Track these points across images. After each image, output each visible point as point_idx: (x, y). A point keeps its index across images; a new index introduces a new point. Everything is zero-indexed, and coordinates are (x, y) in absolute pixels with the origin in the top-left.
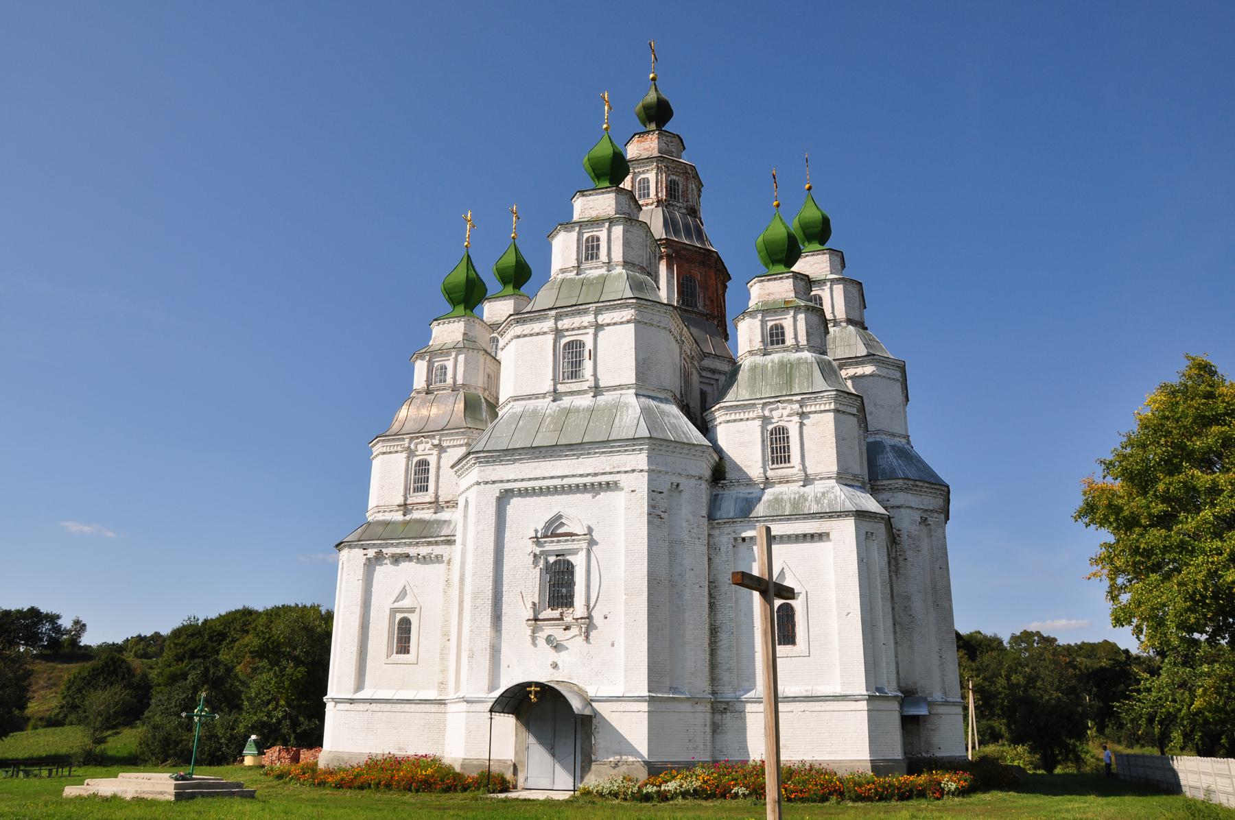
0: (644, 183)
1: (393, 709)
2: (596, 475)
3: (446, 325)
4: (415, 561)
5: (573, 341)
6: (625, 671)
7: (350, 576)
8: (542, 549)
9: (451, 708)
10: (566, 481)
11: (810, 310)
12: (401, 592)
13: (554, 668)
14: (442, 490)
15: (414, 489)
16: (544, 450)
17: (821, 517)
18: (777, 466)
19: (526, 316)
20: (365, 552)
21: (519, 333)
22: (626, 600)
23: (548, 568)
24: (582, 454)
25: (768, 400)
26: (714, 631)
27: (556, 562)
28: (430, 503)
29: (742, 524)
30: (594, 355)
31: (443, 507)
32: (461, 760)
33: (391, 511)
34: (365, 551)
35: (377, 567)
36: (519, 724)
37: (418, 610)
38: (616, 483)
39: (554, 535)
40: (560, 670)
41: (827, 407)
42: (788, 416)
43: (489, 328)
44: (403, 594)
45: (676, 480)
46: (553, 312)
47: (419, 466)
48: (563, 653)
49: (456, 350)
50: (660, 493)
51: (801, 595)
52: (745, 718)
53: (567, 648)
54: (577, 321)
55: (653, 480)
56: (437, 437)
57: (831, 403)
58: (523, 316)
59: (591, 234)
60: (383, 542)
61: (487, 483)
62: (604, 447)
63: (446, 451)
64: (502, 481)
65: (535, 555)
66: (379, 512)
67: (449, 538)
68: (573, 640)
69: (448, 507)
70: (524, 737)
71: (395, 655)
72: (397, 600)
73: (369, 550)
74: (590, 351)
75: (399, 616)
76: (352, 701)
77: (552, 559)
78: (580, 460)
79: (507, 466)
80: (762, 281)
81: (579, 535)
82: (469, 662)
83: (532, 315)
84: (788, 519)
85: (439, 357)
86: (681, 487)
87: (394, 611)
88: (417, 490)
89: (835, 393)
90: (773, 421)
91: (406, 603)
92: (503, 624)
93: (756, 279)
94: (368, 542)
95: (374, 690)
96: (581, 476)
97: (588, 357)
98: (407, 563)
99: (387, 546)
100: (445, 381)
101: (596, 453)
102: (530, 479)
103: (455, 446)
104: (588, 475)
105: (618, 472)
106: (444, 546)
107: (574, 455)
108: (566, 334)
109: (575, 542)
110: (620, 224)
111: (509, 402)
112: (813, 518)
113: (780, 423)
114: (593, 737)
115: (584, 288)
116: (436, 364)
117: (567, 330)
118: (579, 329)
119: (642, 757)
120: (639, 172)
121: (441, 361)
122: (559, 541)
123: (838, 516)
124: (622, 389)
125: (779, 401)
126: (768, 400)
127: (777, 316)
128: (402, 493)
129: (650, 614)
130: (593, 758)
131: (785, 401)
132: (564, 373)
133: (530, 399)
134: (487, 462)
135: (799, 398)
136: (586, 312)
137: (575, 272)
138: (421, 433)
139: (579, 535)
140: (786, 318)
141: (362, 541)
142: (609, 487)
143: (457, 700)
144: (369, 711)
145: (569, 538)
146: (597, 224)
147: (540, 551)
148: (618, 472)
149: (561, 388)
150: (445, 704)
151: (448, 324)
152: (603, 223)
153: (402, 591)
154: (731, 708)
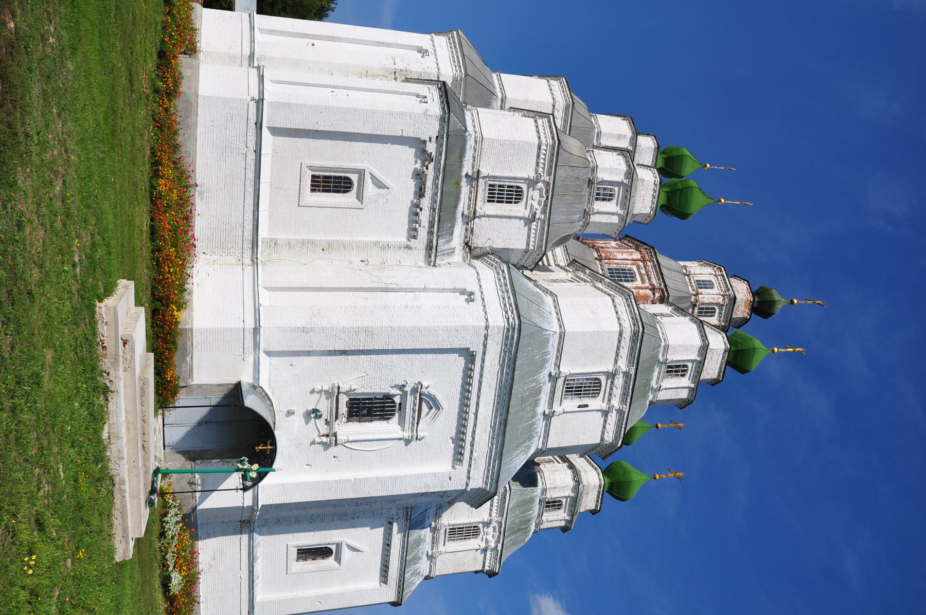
0: (710, 285)
1: (248, 183)
2: (472, 445)
3: (653, 186)
4: (415, 201)
5: (600, 386)
7: (408, 118)
8: (409, 393)
10: (471, 417)
12: (381, 183)
14: (485, 221)
15: (493, 186)
16: (506, 398)
17: (400, 581)
18: (447, 536)
19: (638, 345)
20: (434, 139)
21: (624, 335)
22: (350, 480)
23: (388, 397)
24: (494, 431)
25: (503, 526)
27: (394, 402)
31: (467, 224)
33: (474, 158)
34: (435, 139)
35: (414, 150)
36: (231, 387)
38: (461, 461)
39: (421, 400)
40: (285, 418)
41: (487, 564)
42: (486, 539)
44: (380, 185)
46: (633, 372)
48: (303, 420)
49: (625, 215)
51: (338, 565)
52: (235, 534)
53: (307, 424)
54: (618, 392)
56: (542, 217)
57: (489, 567)
58: (639, 341)
60: (442, 167)
61: (486, 338)
62: (496, 454)
63: (525, 225)
64: (484, 354)
65: (404, 386)
66: (476, 142)
67: (434, 250)
69: (467, 230)
70: (217, 393)
71: (310, 173)
72: (373, 177)
73: (435, 145)
74: (587, 406)
75: (354, 178)
76: (259, 125)
77: (397, 400)
78: (489, 429)
79: (498, 356)
80: (600, 487)
82: (298, 328)
83: (637, 351)
84: (402, 559)
85: (623, 193)
87: (361, 173)
90: (485, 528)
91: (369, 188)
92: (336, 357)
93: (603, 483)
94: (444, 146)
96: (474, 432)
97: (582, 403)
98: (413, 189)
99: (437, 169)
101: (492, 444)
102: (480, 383)
103: (529, 237)
104: (473, 439)
105: (470, 465)
106: (425, 241)
107: (495, 424)
108: (609, 381)
109: (411, 425)
110: (688, 396)
112: (400, 575)
113: (482, 533)
114: (219, 460)
116: (616, 189)
117: (612, 383)
118: (610, 394)
119: (200, 504)
120: (722, 309)
121: (618, 195)
122: (414, 411)
123: (399, 593)
124: (544, 438)
125: (500, 533)
126: (503, 526)
127: (569, 506)
128: (491, 174)
130: (198, 462)
131: (499, 538)
132: (574, 380)
133: (558, 351)
134: (507, 338)
135: (499, 548)
136: (623, 401)
140: (565, 512)
142: (458, 456)
144: (246, 149)
145: (416, 421)
146: (696, 377)
147: (407, 392)
148: (470, 465)
150: (253, 263)
151: (652, 201)
152: (695, 382)
153: (383, 184)
154: (244, 525)
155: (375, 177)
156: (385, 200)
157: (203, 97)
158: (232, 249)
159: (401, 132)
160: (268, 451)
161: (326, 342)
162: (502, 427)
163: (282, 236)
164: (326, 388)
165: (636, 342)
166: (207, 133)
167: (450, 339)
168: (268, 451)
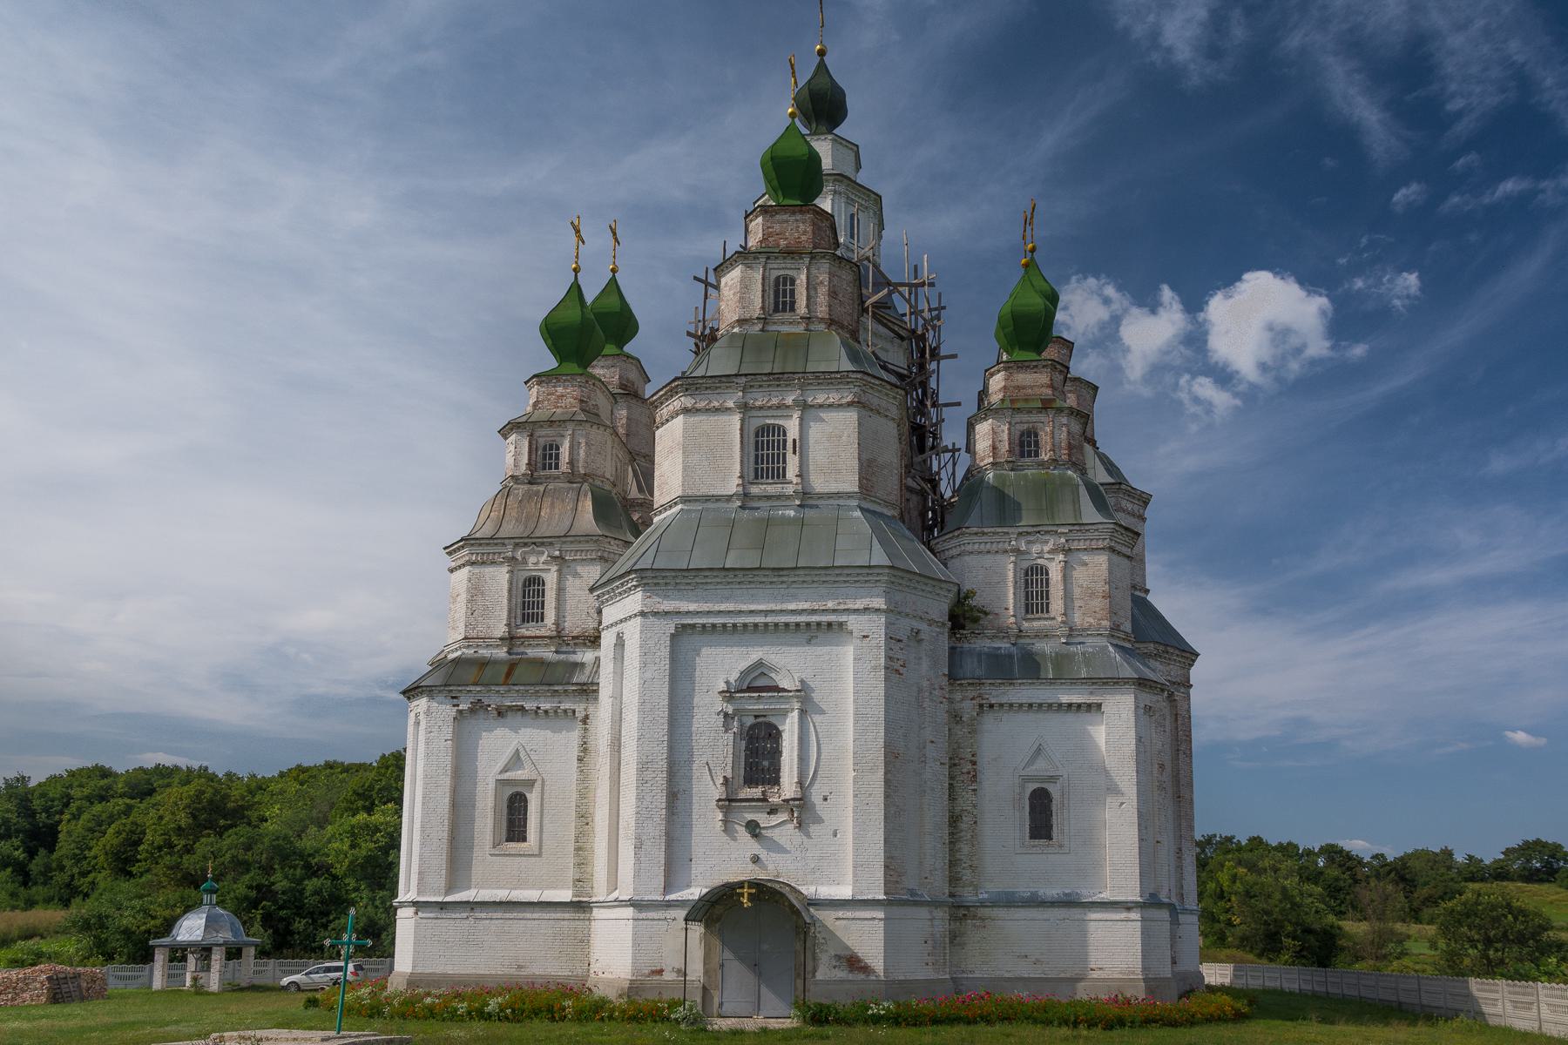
6: (854, 867)
9: (597, 913)
11: (1075, 414)
13: (754, 862)
18: (1037, 616)
22: (855, 778)
26: (954, 820)
28: (551, 638)
29: (1022, 687)
30: (801, 447)
32: (629, 982)
37: (538, 784)
38: (841, 624)
42: (543, 563)
43: (611, 398)
44: (516, 760)
45: (916, 624)
47: (530, 586)
50: (899, 641)
55: (891, 624)
59: (782, 272)
65: (726, 715)
68: (781, 829)
74: (794, 441)
75: (509, 791)
76: (442, 906)
77: (750, 721)
81: (791, 691)
82: (635, 854)
86: (922, 636)
87: (501, 783)
88: (526, 618)
89: (1112, 526)
95: (476, 891)
100: (557, 467)
111: (676, 503)
113: (1040, 561)
115: (778, 349)
129: (887, 796)
131: (1047, 532)
137: (760, 326)
138: (531, 538)
139: (791, 691)
141: (450, 685)
143: (616, 903)
149: (755, 490)
155: (504, 767)
156: (532, 752)
157: (414, 967)
158: (584, 932)
159: (448, 742)
160: (751, 891)
161: (655, 820)
162: (785, 573)
163: (571, 874)
164: (720, 816)
165: (698, 386)
166: (453, 963)
167: (657, 660)
168: (751, 891)
